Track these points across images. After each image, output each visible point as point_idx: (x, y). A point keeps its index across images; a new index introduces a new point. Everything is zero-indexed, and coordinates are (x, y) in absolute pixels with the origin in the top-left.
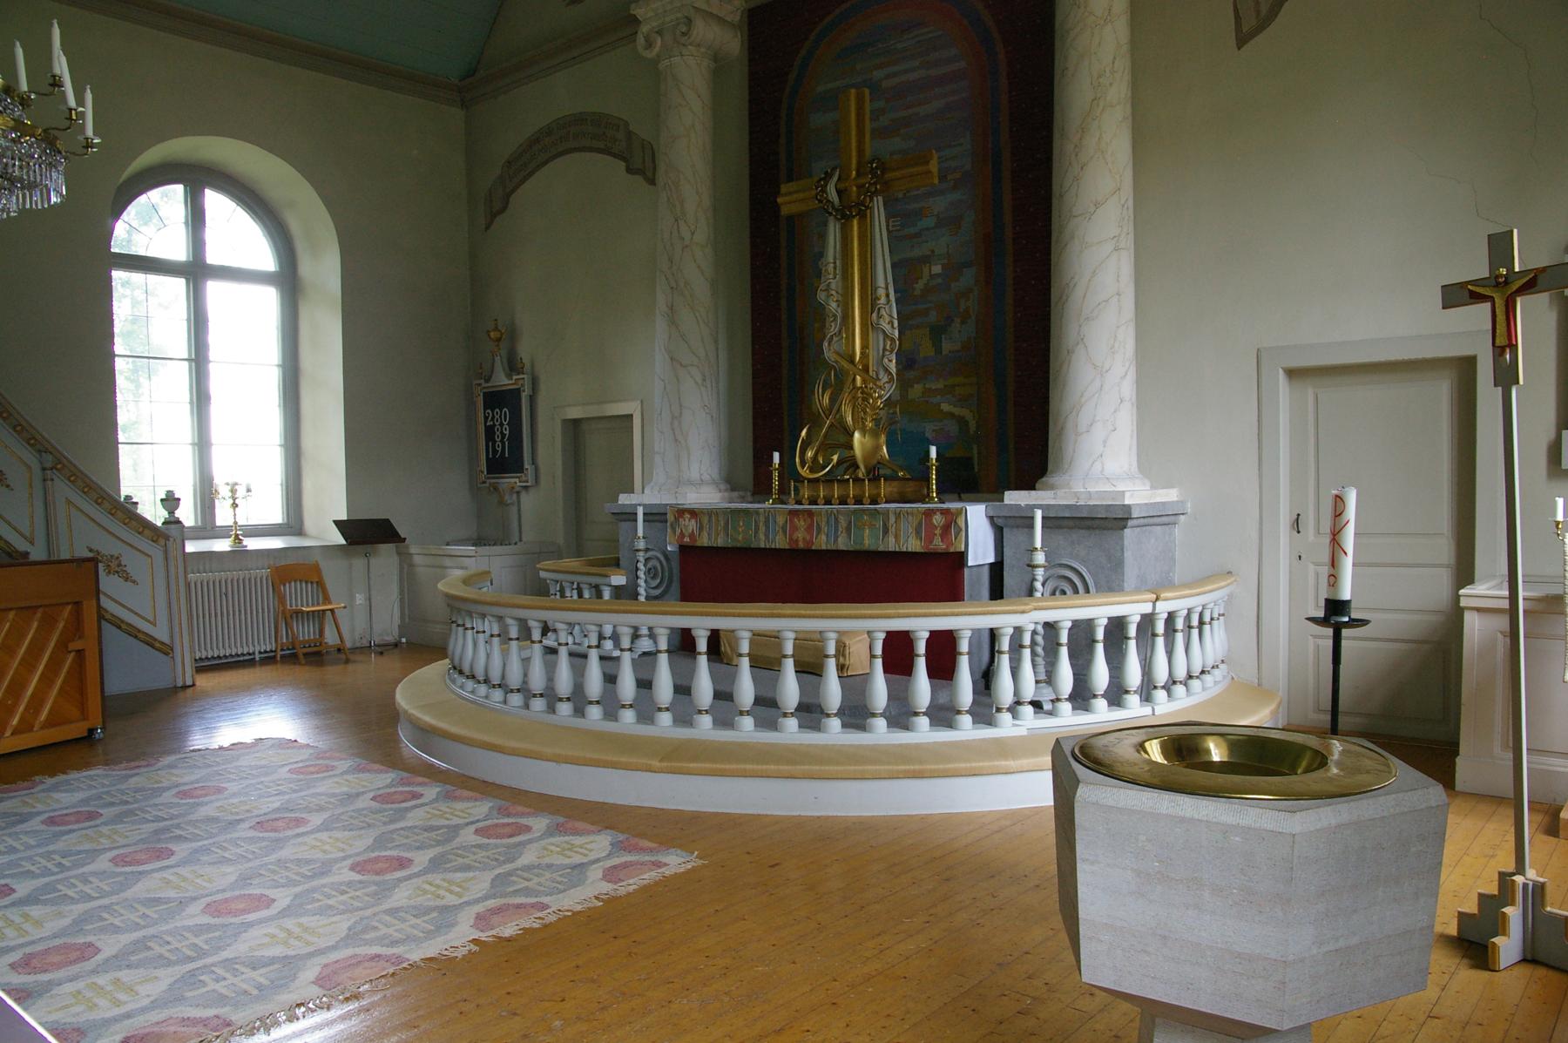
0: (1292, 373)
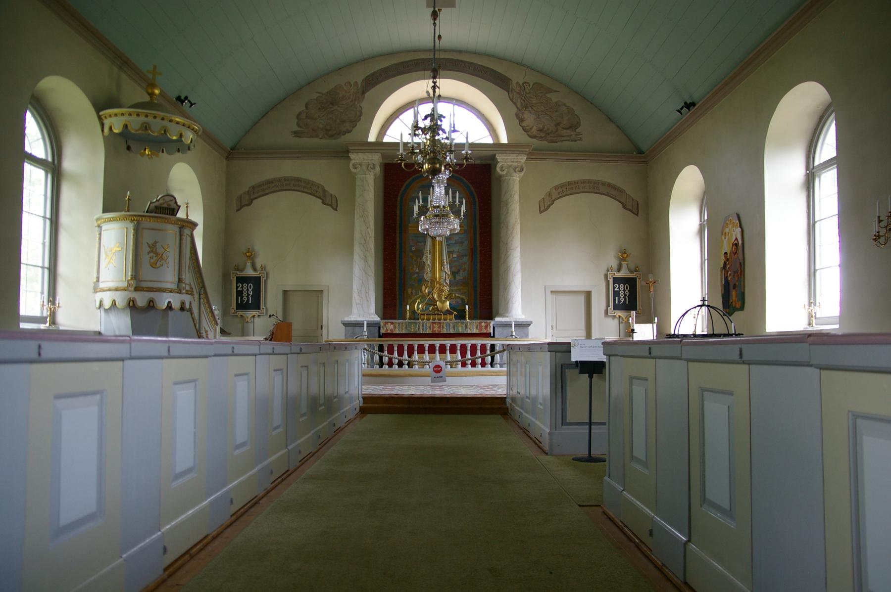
0: (552, 292)
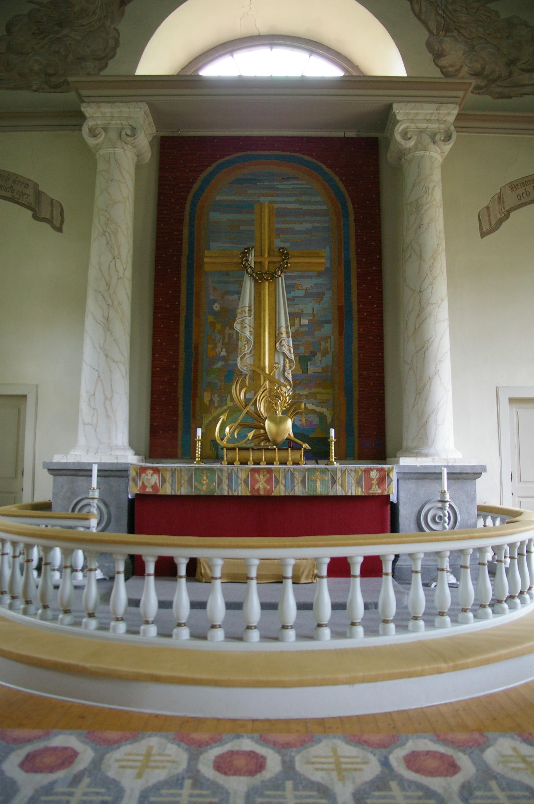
0: (512, 401)
